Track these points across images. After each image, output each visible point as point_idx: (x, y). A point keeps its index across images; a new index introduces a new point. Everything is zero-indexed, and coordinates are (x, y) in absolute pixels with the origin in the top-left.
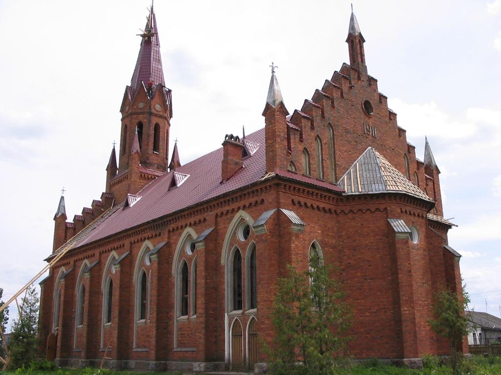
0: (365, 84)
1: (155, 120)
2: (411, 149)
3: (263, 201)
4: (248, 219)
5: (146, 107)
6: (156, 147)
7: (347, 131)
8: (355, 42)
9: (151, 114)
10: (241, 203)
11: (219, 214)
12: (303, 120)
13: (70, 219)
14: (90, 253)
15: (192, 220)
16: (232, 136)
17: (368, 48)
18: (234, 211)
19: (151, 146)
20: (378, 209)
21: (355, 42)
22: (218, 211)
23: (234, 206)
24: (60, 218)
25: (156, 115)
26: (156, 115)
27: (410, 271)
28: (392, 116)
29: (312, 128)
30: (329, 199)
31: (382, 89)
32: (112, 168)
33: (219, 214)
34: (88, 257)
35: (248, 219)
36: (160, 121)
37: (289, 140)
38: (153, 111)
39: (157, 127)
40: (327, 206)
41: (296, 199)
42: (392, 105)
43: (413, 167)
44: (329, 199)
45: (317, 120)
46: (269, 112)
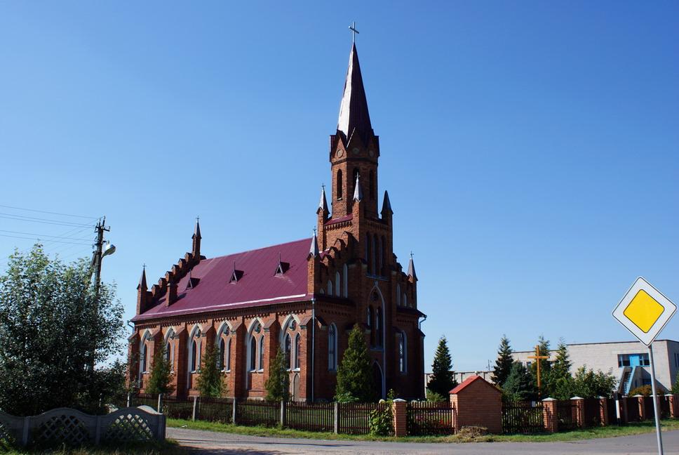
8: (197, 239)
13: (149, 290)
21: (197, 239)
24: (143, 286)
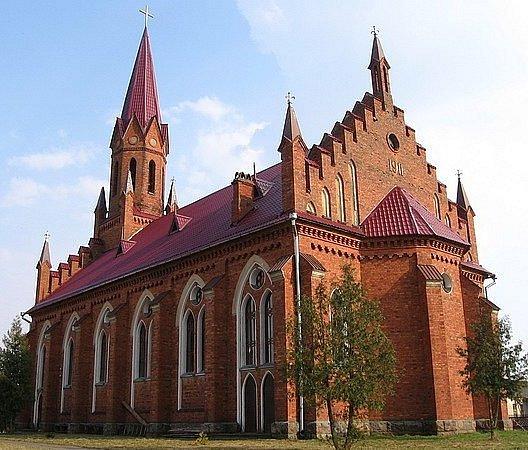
0: (390, 115)
1: (149, 157)
2: (441, 187)
3: (279, 245)
4: (264, 267)
5: (137, 136)
6: (151, 188)
7: (370, 168)
8: (378, 67)
9: (144, 149)
10: (255, 248)
11: (230, 259)
12: (323, 155)
14: (81, 304)
15: (199, 267)
16: (243, 175)
17: (393, 76)
18: (246, 256)
19: (146, 186)
20: (406, 255)
21: (378, 67)
22: (229, 256)
23: (246, 250)
25: (151, 151)
26: (151, 151)
27: (443, 323)
28: (420, 150)
29: (333, 164)
30: (314, 233)
31: (409, 121)
32: (100, 210)
33: (230, 259)
34: (77, 310)
35: (264, 267)
36: (156, 158)
37: (307, 177)
38: (148, 146)
39: (152, 164)
40: (350, 252)
41: (316, 242)
42: (421, 138)
43: (445, 208)
44: (314, 233)
45: (338, 155)
46: (285, 147)
